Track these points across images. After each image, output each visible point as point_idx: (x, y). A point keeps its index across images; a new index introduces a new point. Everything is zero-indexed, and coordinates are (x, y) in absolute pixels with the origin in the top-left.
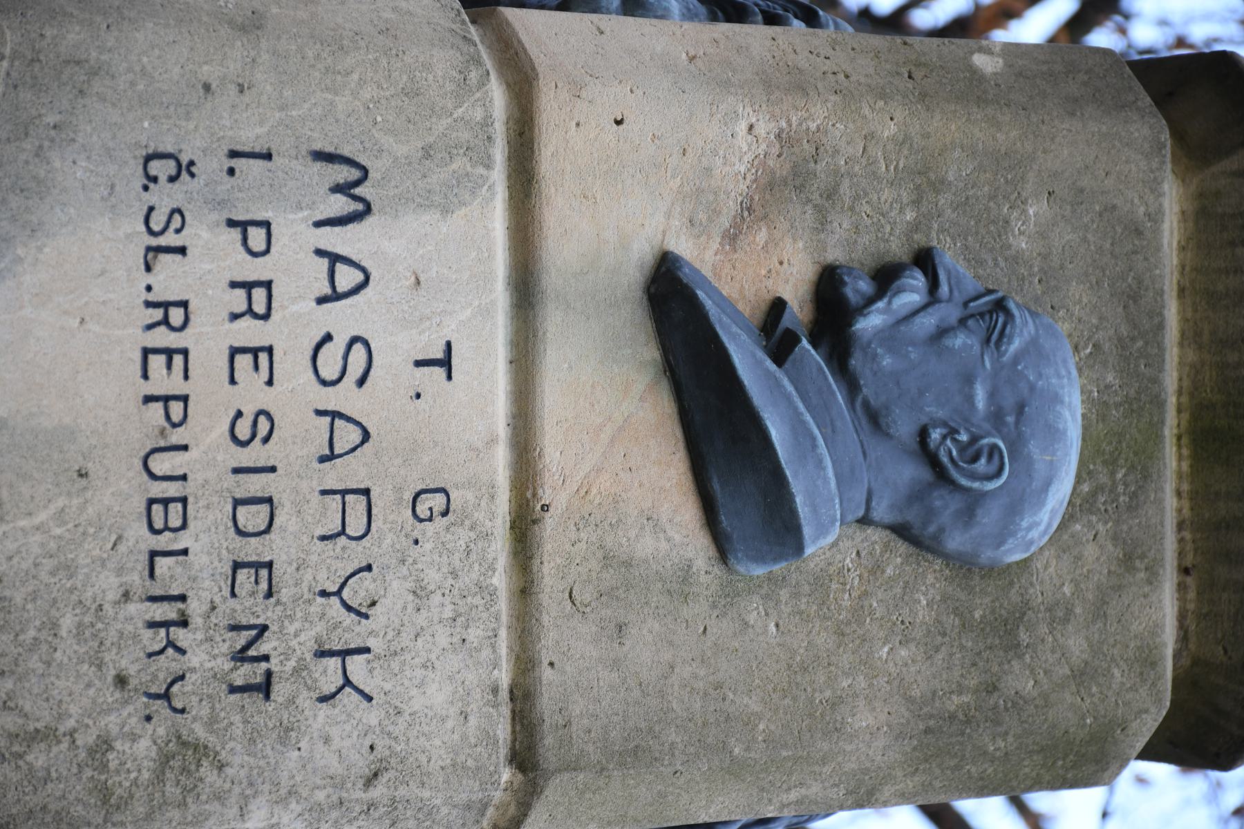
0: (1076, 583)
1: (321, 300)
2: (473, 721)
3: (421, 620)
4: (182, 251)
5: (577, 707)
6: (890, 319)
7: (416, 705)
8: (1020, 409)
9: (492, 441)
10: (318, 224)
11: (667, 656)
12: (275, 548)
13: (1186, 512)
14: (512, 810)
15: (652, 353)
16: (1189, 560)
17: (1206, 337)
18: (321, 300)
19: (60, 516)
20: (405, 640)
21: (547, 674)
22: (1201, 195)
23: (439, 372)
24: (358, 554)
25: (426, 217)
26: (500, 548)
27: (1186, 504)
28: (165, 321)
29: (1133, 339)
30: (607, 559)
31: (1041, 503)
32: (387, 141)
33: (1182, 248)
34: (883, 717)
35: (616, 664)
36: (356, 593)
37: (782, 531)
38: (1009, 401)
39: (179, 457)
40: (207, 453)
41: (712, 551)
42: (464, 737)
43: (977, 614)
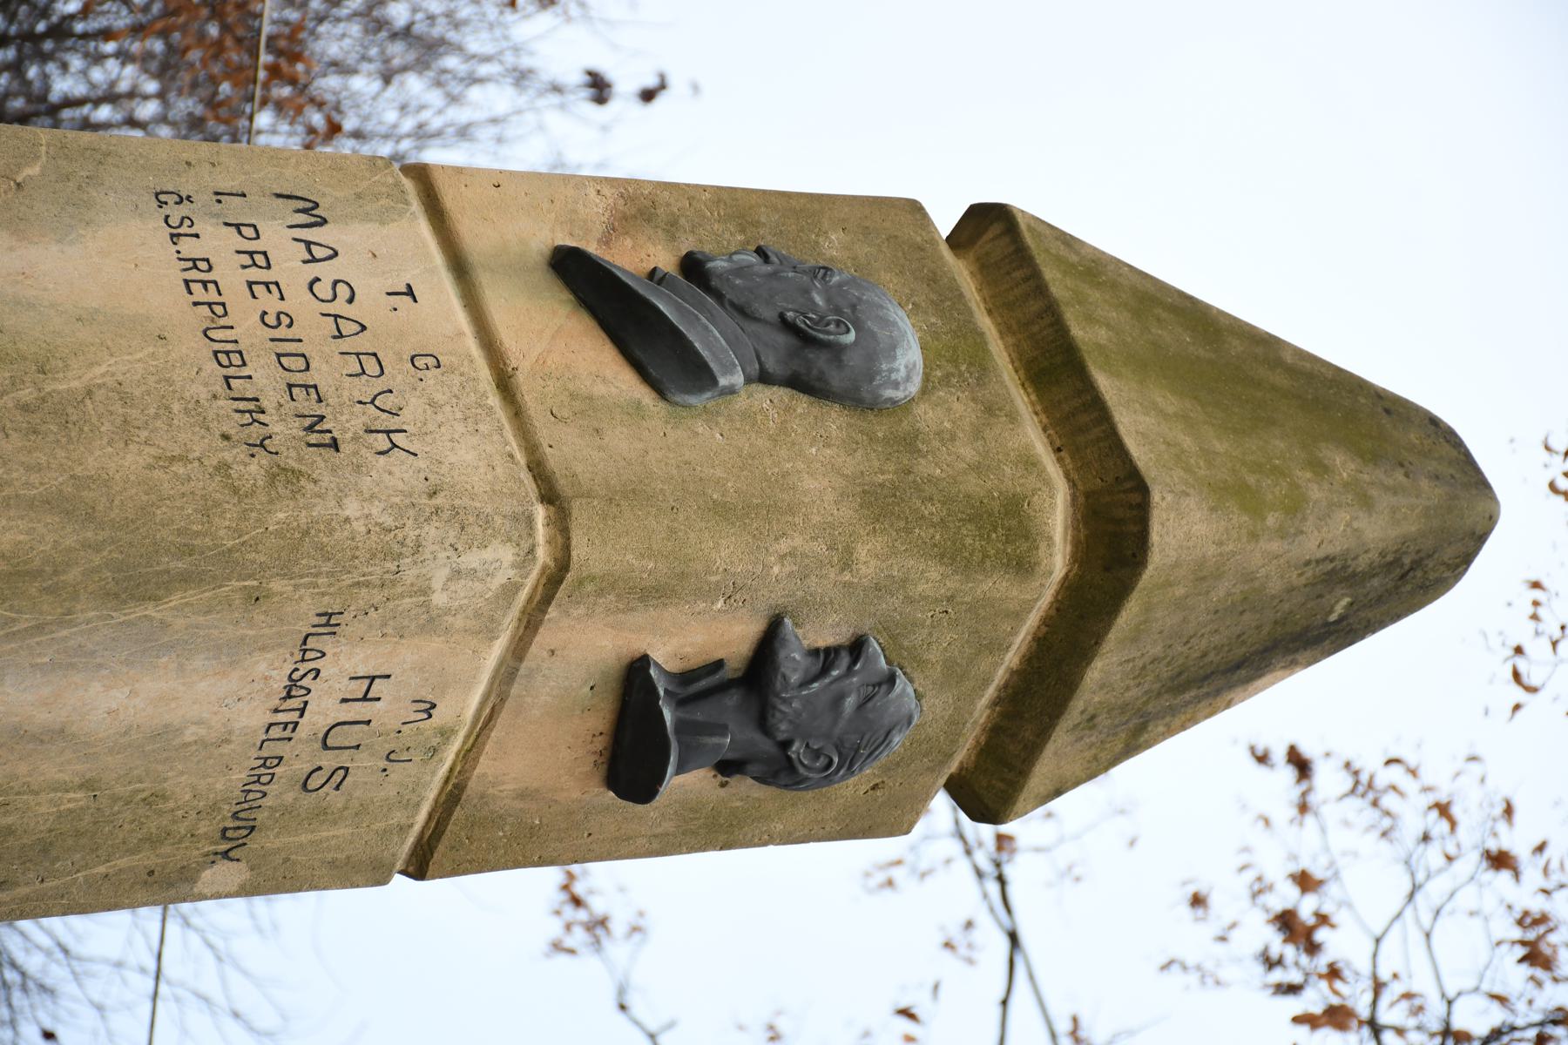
1: (305, 262)
2: (499, 470)
5: (579, 469)
7: (453, 459)
10: (291, 227)
11: (640, 446)
13: (1045, 420)
14: (560, 540)
15: (566, 295)
16: (1058, 443)
17: (1015, 327)
18: (305, 262)
22: (978, 259)
25: (369, 225)
26: (494, 400)
28: (195, 267)
30: (573, 396)
32: (327, 190)
33: (979, 291)
34: (826, 483)
35: (600, 448)
36: (385, 401)
37: (698, 375)
39: (229, 332)
41: (654, 395)
43: (880, 435)
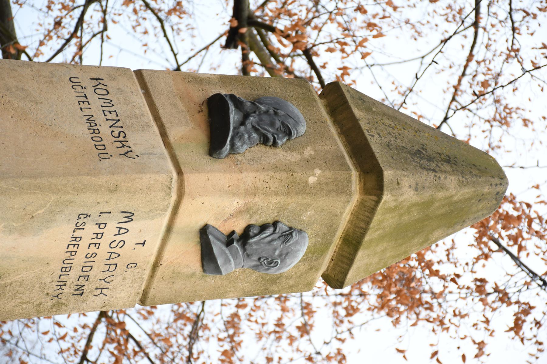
0: (296, 273)
2: (131, 298)
3: (123, 283)
4: (83, 229)
6: (259, 239)
8: (287, 254)
9: (152, 255)
12: (91, 274)
13: (337, 250)
15: (198, 240)
19: (40, 271)
20: (118, 286)
21: (152, 290)
23: (142, 245)
24: (107, 285)
27: (337, 249)
29: (328, 233)
31: (294, 257)
38: (285, 252)
40: (79, 259)
42: (128, 301)
